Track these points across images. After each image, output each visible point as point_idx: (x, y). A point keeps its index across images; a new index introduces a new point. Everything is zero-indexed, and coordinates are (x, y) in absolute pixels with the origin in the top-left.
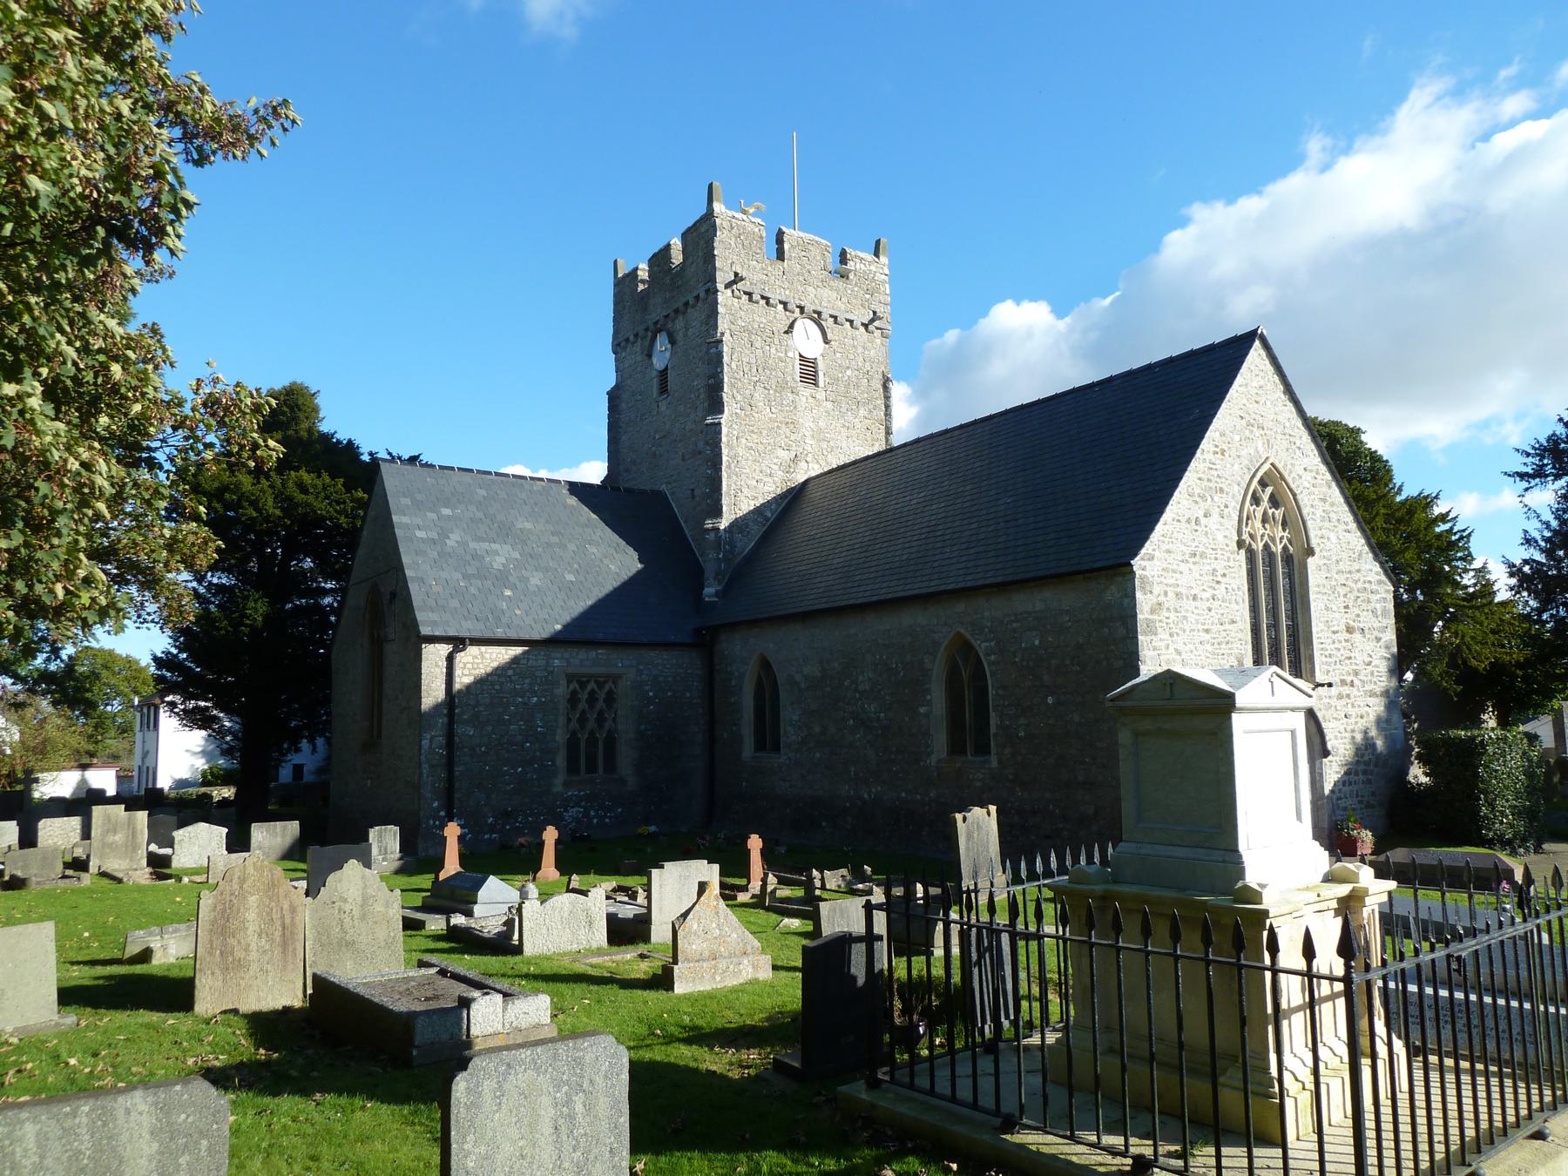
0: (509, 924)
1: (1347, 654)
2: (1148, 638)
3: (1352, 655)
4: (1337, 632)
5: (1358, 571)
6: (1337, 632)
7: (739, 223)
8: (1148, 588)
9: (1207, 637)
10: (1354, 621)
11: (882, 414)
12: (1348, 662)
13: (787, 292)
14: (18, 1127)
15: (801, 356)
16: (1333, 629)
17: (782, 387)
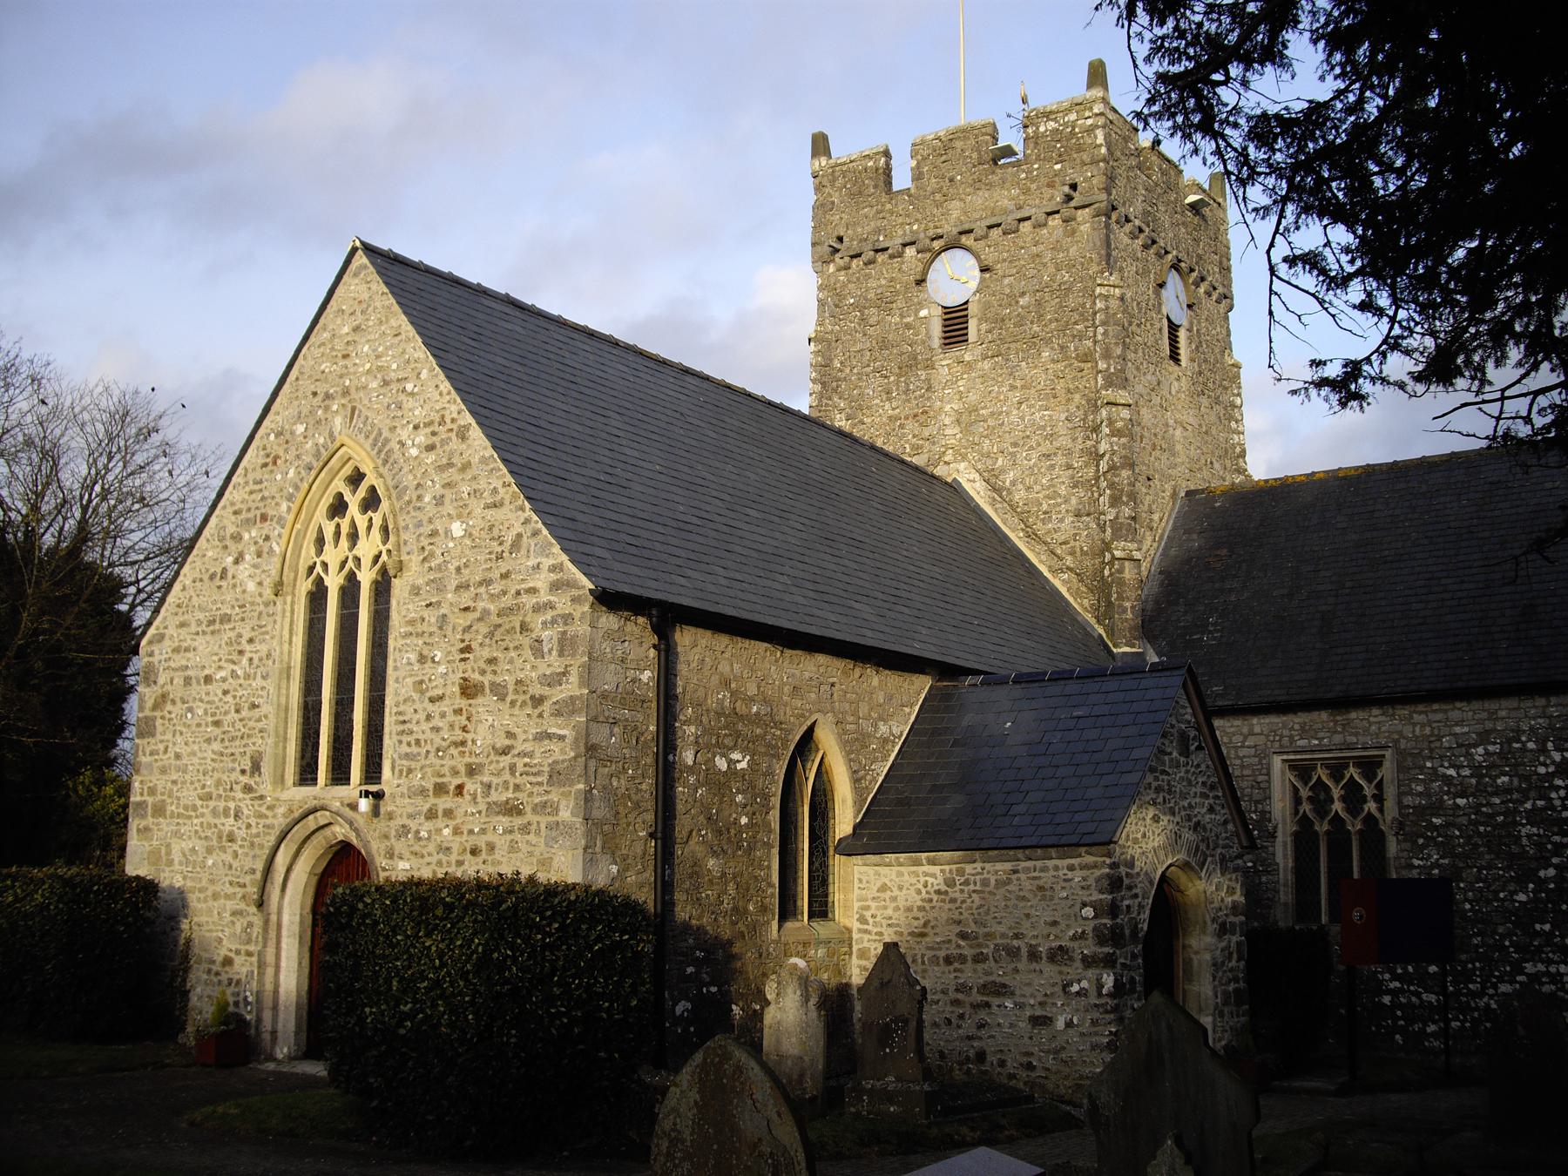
1: (459, 735)
3: (469, 737)
4: (441, 698)
5: (505, 576)
6: (441, 698)
8: (152, 678)
9: (217, 731)
10: (483, 672)
11: (1089, 343)
12: (453, 751)
13: (915, 227)
14: (1235, 70)
16: (429, 694)
17: (910, 364)
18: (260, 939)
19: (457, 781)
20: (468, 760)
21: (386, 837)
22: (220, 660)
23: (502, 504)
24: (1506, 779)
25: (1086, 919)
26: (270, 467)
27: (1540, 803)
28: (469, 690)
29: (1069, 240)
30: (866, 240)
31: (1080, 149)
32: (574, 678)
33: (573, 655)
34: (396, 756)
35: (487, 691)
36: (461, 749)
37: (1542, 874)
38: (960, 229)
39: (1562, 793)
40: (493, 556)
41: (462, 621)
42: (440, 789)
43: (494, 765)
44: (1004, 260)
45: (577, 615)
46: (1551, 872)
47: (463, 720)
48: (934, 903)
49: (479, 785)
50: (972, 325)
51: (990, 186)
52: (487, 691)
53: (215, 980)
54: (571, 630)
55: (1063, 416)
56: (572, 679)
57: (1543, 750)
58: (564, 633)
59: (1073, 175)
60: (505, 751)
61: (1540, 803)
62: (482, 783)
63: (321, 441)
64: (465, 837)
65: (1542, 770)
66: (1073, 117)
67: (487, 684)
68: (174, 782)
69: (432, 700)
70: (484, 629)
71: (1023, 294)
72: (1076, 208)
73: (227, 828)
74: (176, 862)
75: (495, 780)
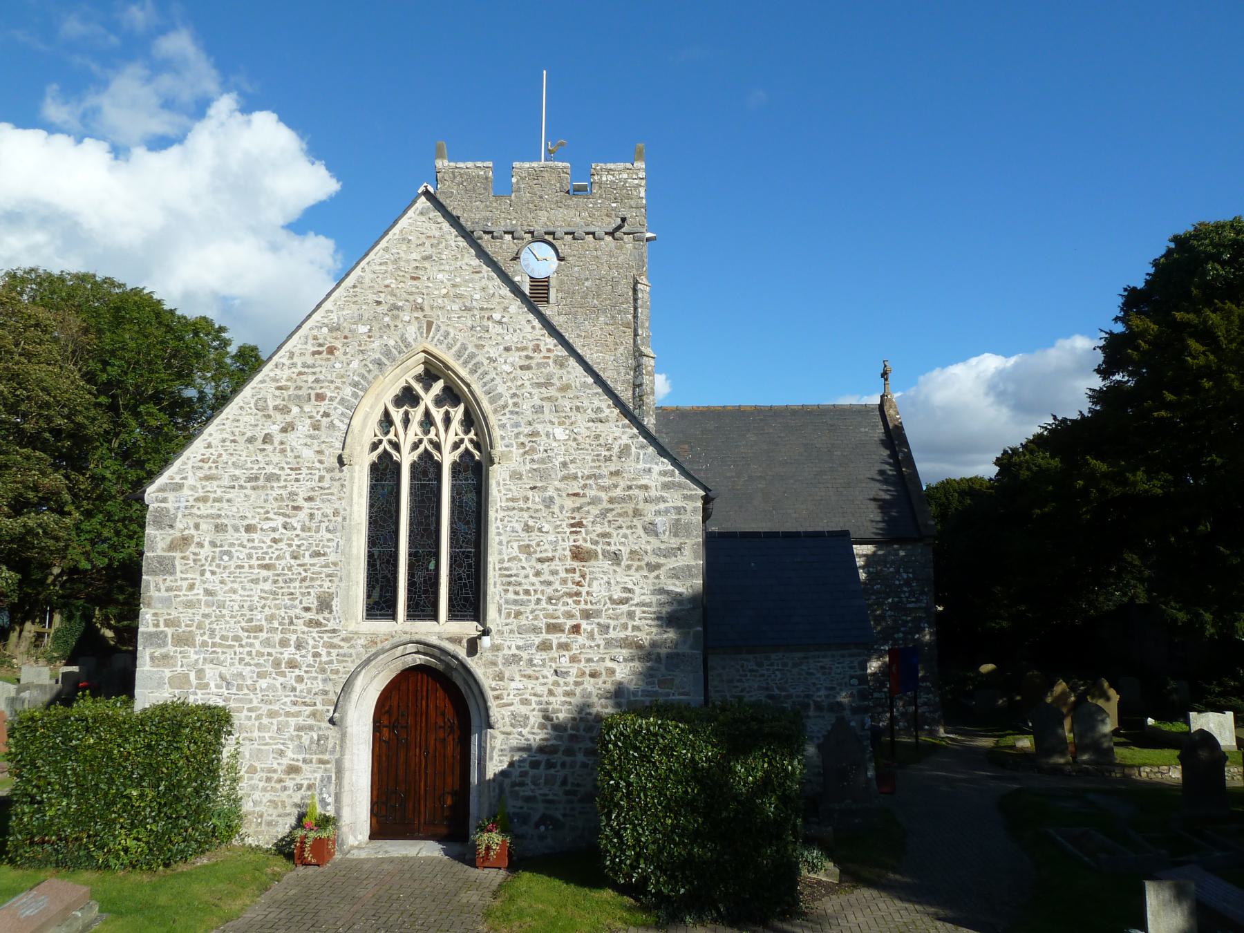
0: (805, 914)
2: (160, 579)
7: (462, 171)
13: (514, 222)
15: (531, 278)
18: (338, 747)
19: (574, 622)
20: (583, 606)
21: (494, 664)
22: (268, 512)
23: (607, 421)
24: (879, 586)
25: (853, 685)
26: (324, 355)
27: (896, 599)
28: (579, 554)
29: (619, 251)
30: (477, 223)
31: (629, 197)
32: (687, 551)
33: (687, 537)
34: (502, 601)
35: (601, 557)
36: (575, 598)
37: (896, 636)
38: (546, 230)
39: (907, 594)
40: (602, 458)
41: (570, 503)
42: (553, 628)
43: (611, 611)
44: (574, 256)
45: (689, 508)
46: (901, 635)
47: (577, 577)
48: (748, 677)
49: (594, 626)
50: (553, 293)
51: (568, 207)
52: (601, 557)
53: (278, 786)
54: (685, 518)
55: (612, 358)
56: (685, 553)
57: (897, 572)
58: (678, 520)
59: (624, 212)
60: (623, 601)
61: (896, 599)
62: (599, 624)
63: (391, 343)
64: (583, 664)
65: (897, 582)
66: (625, 176)
67: (600, 551)
68: (204, 616)
69: (540, 560)
70: (595, 511)
71: (587, 279)
72: (625, 234)
73: (286, 656)
74: (212, 685)
75: (612, 623)
